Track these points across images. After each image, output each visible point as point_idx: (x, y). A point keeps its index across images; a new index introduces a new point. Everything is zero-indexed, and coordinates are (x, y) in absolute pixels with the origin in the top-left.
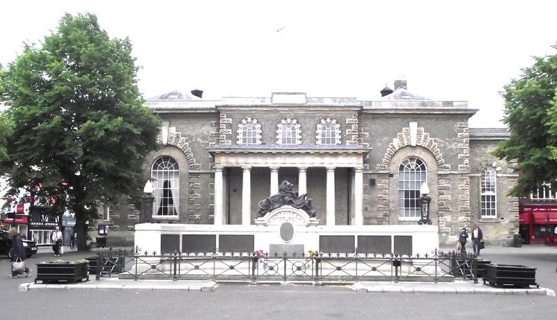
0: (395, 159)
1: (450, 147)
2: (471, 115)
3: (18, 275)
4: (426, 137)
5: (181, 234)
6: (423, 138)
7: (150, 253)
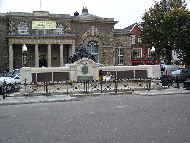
0: (86, 41)
1: (107, 36)
2: (115, 24)
3: (15, 93)
4: (98, 32)
5: (37, 73)
6: (97, 32)
7: (156, 79)
